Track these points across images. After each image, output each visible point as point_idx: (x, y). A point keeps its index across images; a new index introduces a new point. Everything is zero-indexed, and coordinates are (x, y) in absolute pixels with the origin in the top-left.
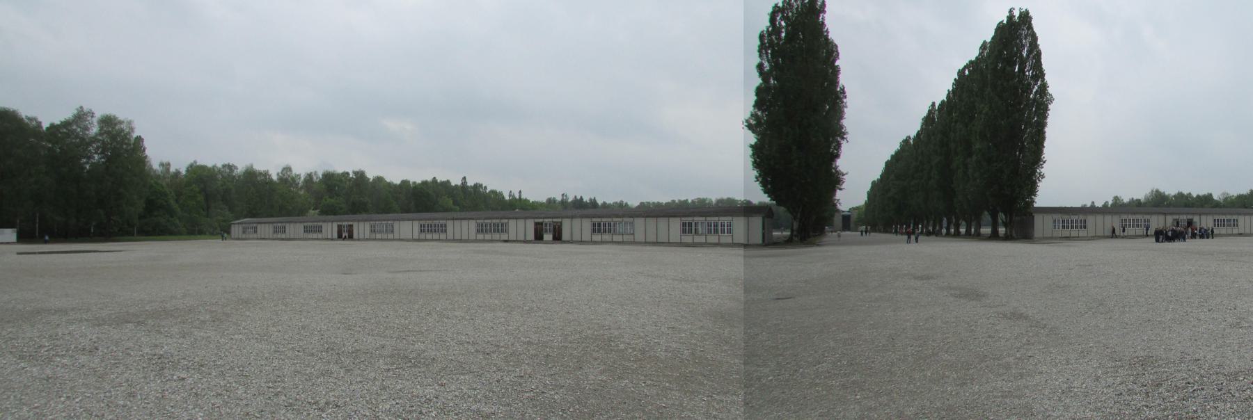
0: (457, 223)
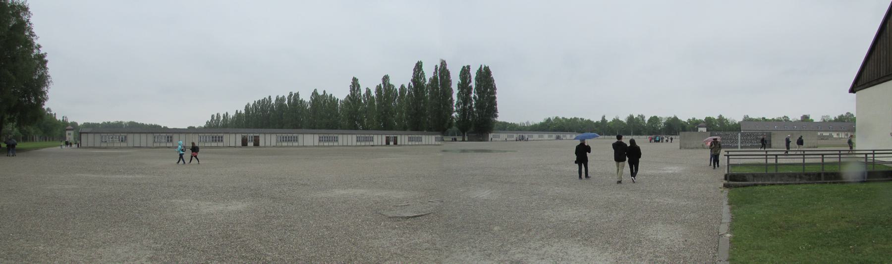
0: (345, 136)
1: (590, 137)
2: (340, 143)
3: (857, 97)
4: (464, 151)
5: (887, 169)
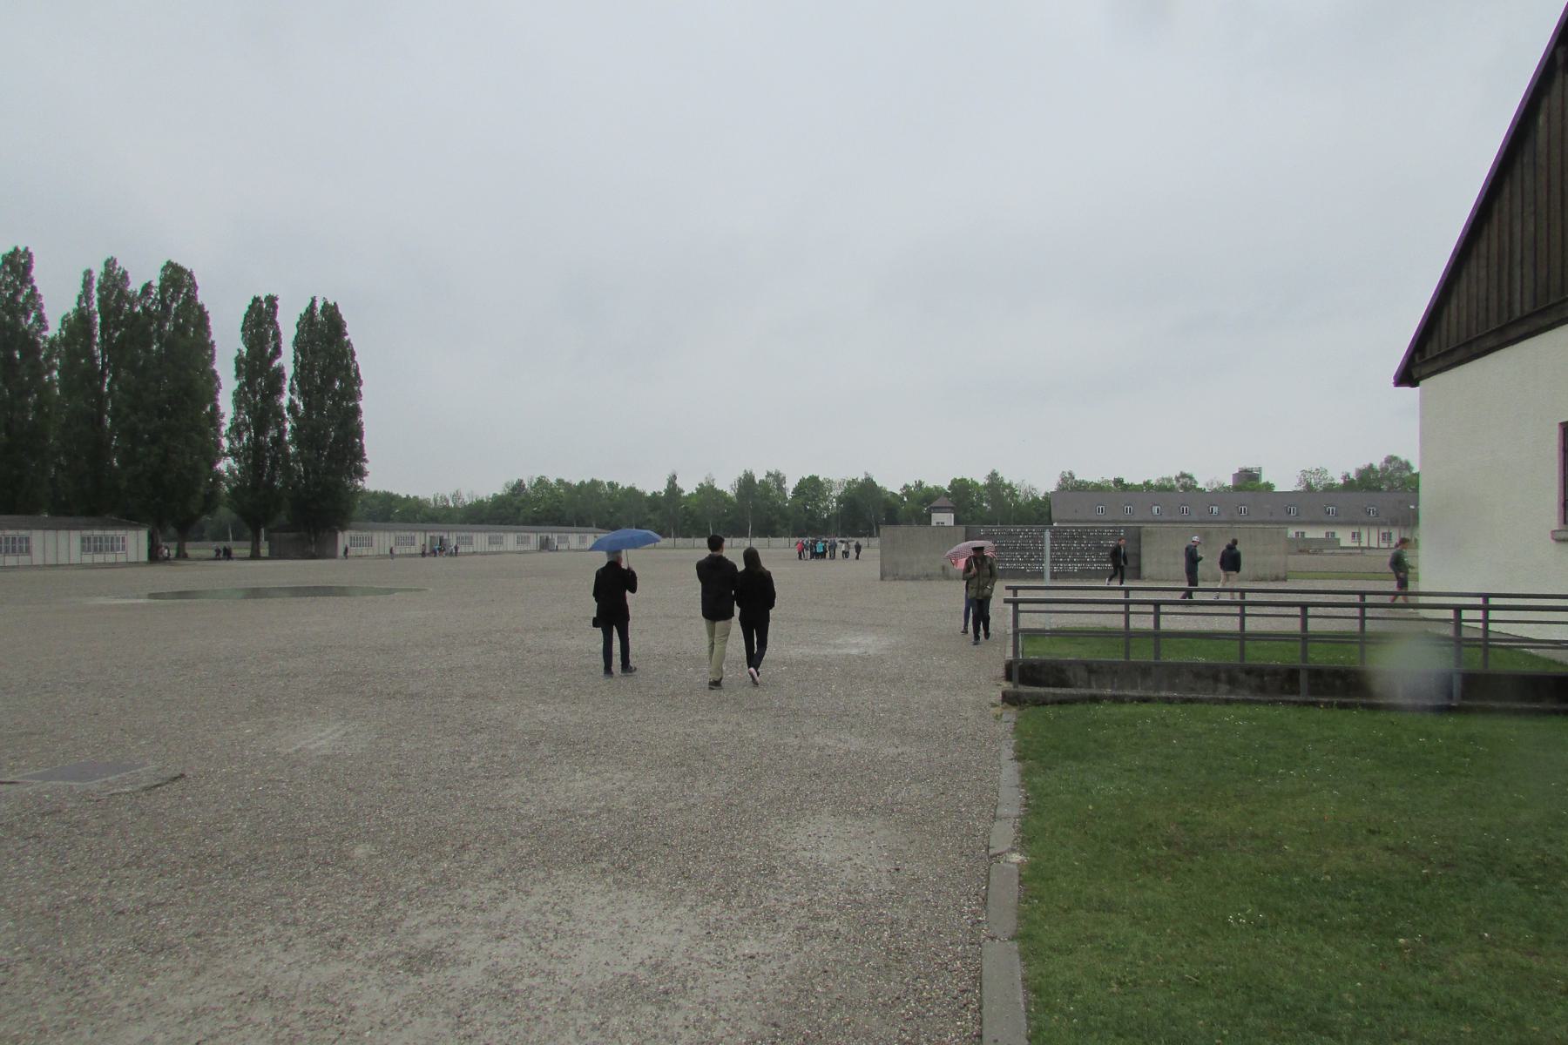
1: (635, 544)
2: (37, 558)
3: (1423, 400)
4: (256, 593)
5: (1538, 669)
